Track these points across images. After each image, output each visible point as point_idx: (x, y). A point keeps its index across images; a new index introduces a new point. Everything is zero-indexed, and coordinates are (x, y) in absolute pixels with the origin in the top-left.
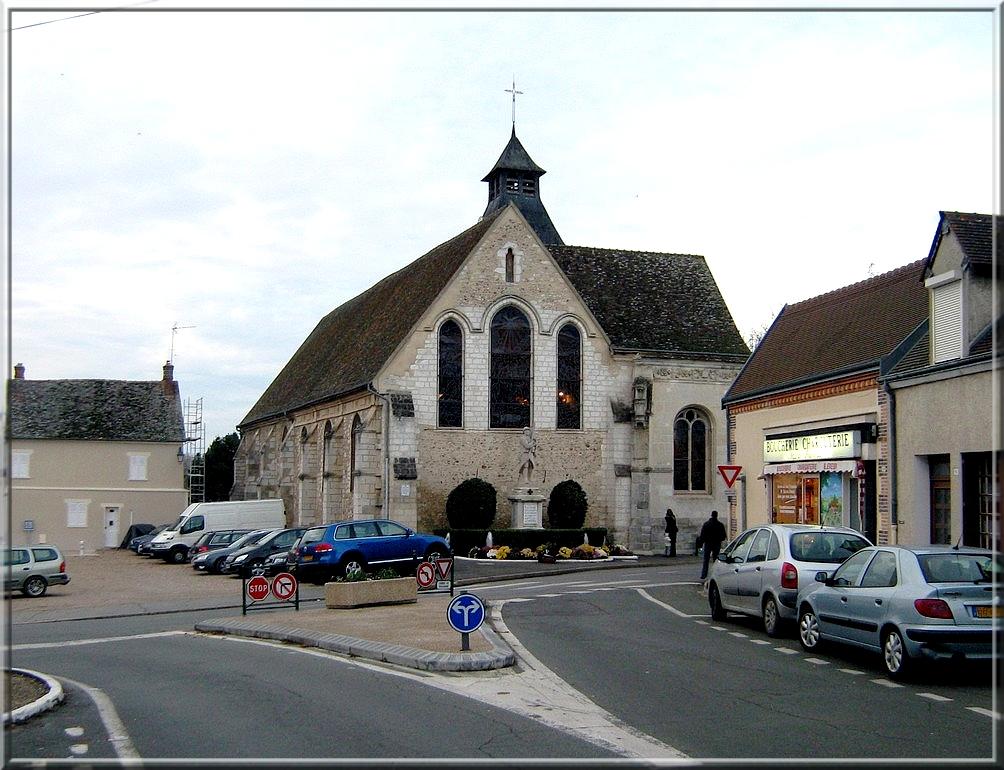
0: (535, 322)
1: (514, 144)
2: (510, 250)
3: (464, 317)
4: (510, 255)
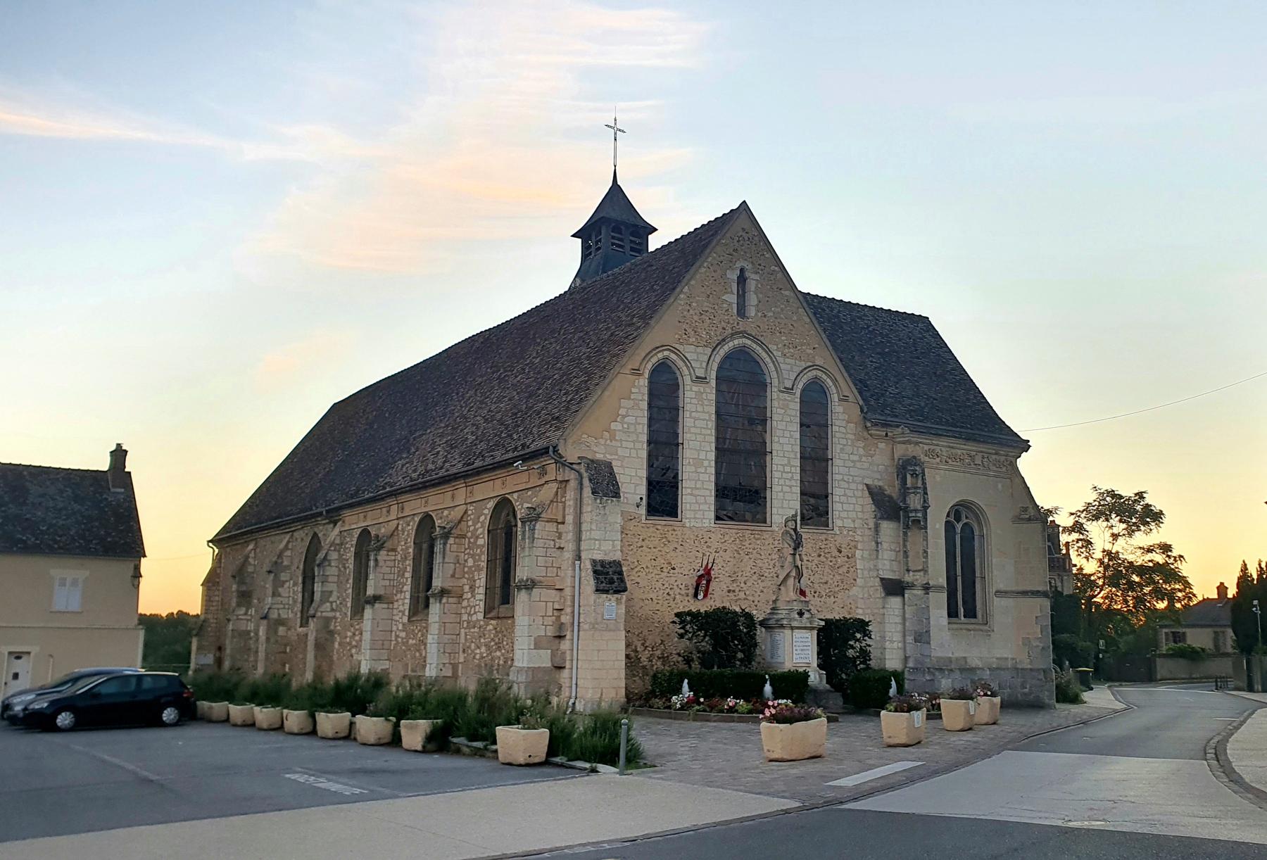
0: (774, 374)
1: (615, 194)
2: (742, 270)
3: (685, 359)
4: (742, 280)
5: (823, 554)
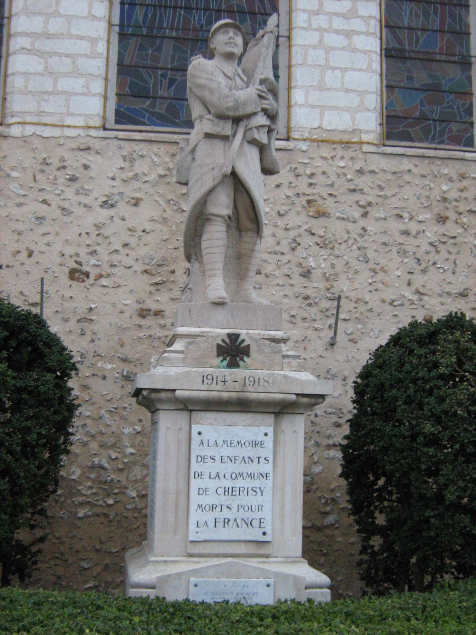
5: (452, 216)
